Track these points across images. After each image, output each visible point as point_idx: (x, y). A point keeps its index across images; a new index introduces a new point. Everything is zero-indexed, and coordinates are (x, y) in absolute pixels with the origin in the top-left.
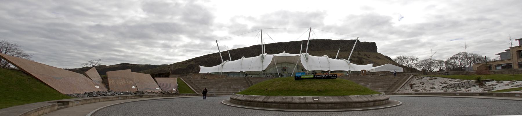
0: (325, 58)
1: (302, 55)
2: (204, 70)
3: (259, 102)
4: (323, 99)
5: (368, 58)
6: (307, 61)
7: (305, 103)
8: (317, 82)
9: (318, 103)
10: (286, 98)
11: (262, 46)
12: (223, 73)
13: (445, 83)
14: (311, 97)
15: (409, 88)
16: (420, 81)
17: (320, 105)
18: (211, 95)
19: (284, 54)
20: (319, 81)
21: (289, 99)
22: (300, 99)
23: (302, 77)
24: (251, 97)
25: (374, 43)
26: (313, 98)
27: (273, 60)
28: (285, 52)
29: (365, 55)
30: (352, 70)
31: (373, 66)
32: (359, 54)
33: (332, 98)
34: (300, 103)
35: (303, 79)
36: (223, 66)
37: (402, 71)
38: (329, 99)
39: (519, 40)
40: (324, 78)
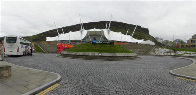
0: (120, 33)
1: (105, 31)
2: (49, 39)
3: (73, 55)
4: (104, 54)
5: (144, 37)
6: (109, 34)
7: (94, 56)
8: (104, 45)
9: (101, 56)
10: (85, 53)
11: (81, 24)
12: (59, 41)
13: (166, 51)
14: (98, 53)
15: (153, 52)
16: (158, 49)
17: (101, 57)
18: (53, 53)
19: (95, 30)
20: (105, 45)
21: (87, 53)
22: (92, 54)
23: (96, 43)
24: (69, 53)
25: (148, 29)
26: (99, 54)
27: (87, 33)
28: (96, 28)
29: (143, 35)
30: (133, 42)
31: (144, 41)
32: (140, 34)
33: (109, 54)
34: (92, 56)
35: (96, 44)
36: (59, 37)
37: (154, 44)
38: (107, 54)
39: (192, 36)
40: (108, 44)
